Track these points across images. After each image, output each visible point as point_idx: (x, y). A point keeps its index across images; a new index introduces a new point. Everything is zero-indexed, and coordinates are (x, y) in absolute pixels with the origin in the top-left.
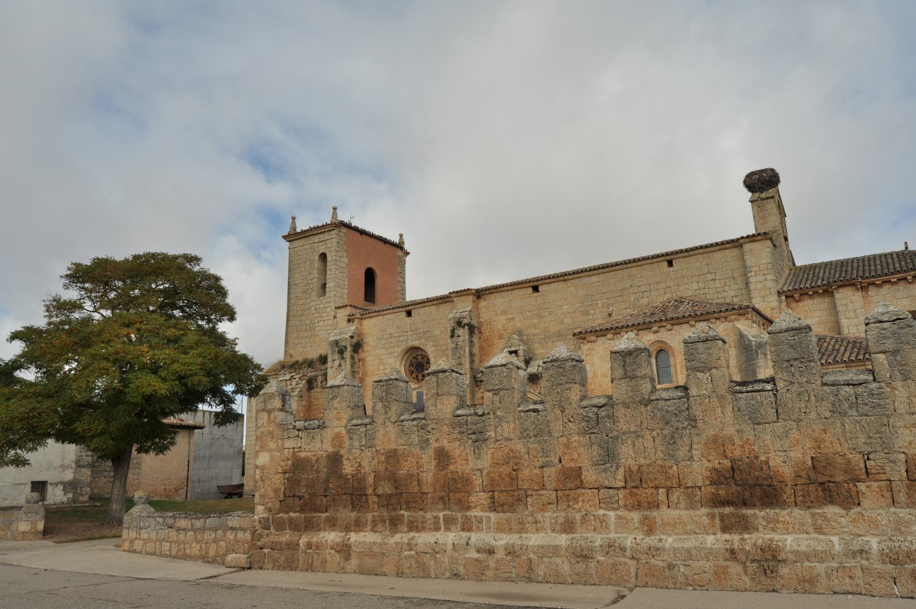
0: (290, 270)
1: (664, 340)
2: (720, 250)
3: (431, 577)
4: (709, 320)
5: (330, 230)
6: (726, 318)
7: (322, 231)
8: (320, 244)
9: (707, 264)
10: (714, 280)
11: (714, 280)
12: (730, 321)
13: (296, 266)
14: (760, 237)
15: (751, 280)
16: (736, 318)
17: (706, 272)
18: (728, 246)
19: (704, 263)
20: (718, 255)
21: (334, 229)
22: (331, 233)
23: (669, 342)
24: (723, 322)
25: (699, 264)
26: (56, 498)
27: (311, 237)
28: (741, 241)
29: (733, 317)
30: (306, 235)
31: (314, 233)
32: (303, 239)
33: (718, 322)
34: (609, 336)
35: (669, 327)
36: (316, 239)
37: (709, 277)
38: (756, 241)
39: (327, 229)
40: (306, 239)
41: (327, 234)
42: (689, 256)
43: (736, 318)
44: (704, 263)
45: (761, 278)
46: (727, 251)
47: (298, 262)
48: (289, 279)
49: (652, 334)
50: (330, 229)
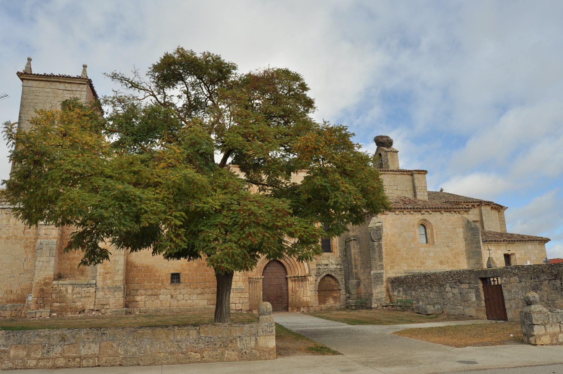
0: (22, 106)
1: (427, 219)
2: (401, 174)
3: (140, 365)
4: (450, 212)
5: (81, 84)
6: (459, 212)
7: (71, 81)
8: (65, 92)
9: (394, 181)
10: (397, 190)
11: (397, 190)
12: (461, 214)
13: (32, 104)
14: (423, 172)
15: (418, 193)
16: (463, 213)
17: (393, 184)
18: (405, 173)
19: (392, 179)
20: (399, 177)
21: (86, 84)
22: (81, 86)
23: (430, 221)
24: (405, 214)
25: (389, 179)
26: (173, 292)
27: (54, 83)
28: (414, 172)
29: (462, 212)
30: (49, 79)
31: (60, 80)
32: (44, 82)
33: (454, 214)
34: (397, 212)
35: (412, 212)
36: (62, 86)
37: (395, 188)
38: (420, 174)
39: (78, 82)
40: (48, 83)
41: (76, 85)
42: (384, 174)
43: (463, 213)
44: (392, 179)
45: (422, 194)
46: (403, 176)
47: (35, 101)
48: (20, 113)
49: (420, 215)
50: (82, 82)
